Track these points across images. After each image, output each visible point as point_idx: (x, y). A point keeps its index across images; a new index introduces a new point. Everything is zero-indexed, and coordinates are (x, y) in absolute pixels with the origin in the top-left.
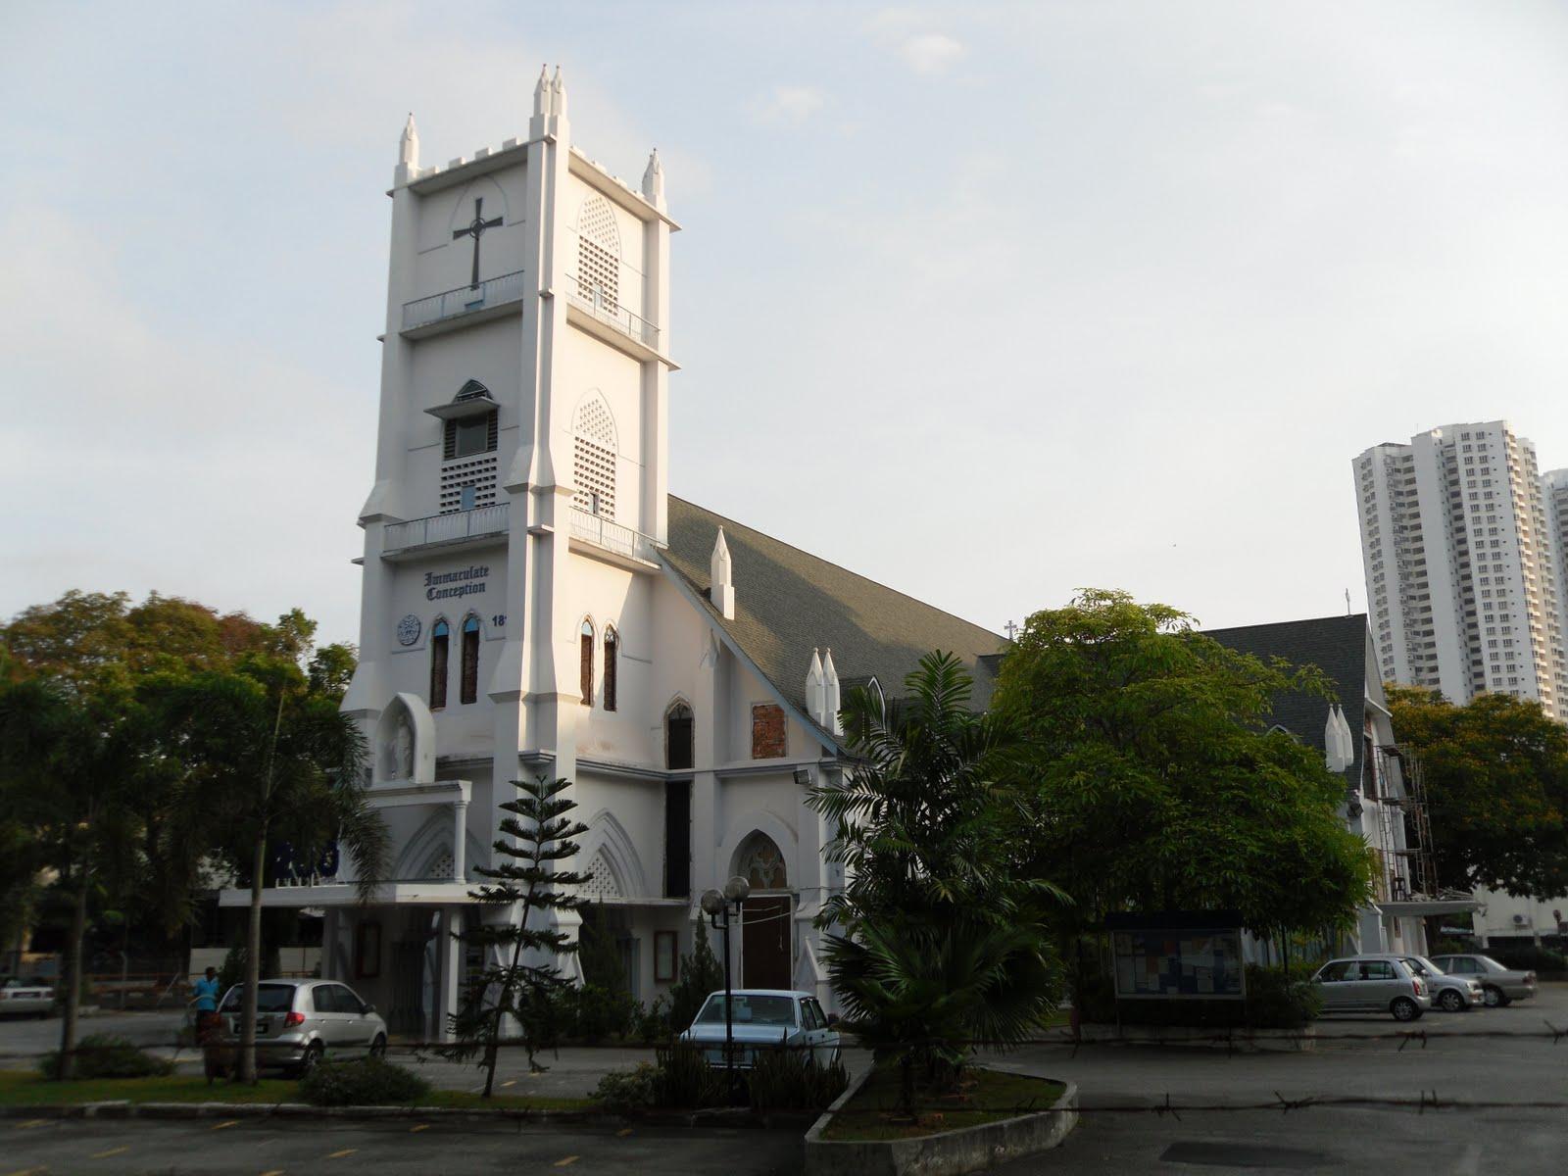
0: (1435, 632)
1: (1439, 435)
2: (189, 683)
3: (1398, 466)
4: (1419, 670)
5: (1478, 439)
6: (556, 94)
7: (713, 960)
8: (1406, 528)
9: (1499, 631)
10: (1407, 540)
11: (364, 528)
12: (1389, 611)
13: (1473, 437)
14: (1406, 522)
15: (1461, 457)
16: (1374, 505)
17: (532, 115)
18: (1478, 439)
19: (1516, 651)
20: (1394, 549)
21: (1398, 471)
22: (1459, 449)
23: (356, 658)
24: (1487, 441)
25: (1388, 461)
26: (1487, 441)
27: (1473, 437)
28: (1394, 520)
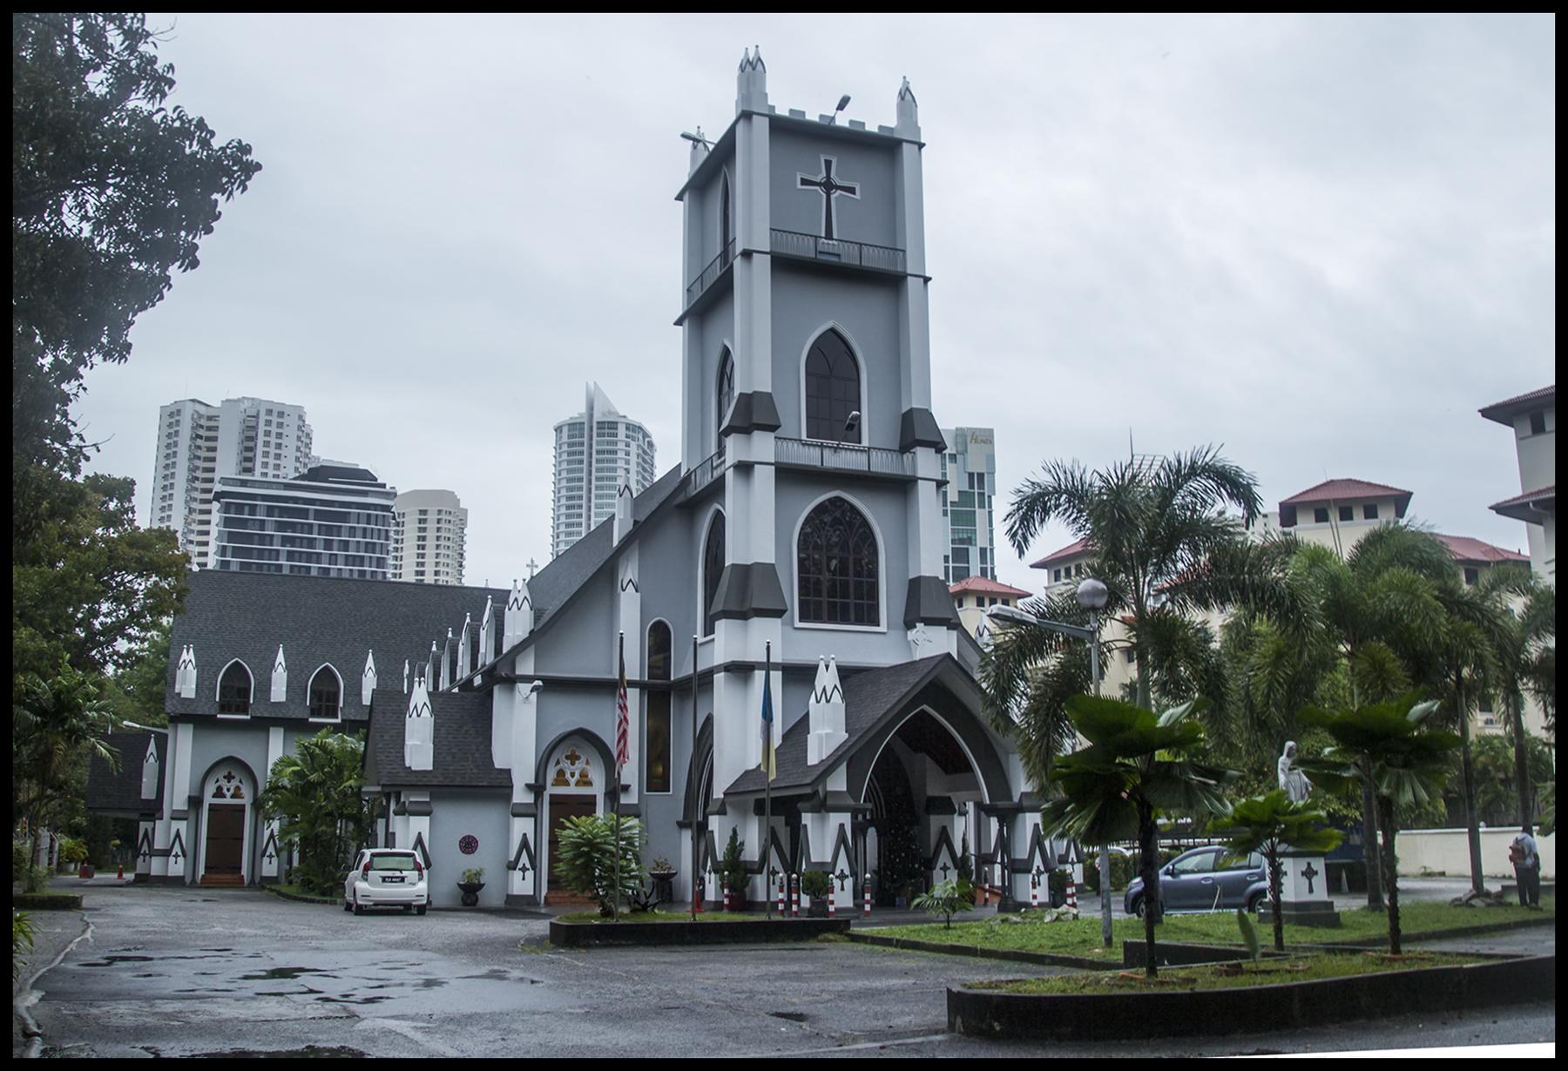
0: (217, 459)
1: (247, 404)
2: (1072, 596)
3: (203, 422)
4: (191, 511)
5: (278, 417)
6: (624, 722)
7: (658, 891)
8: (197, 479)
9: (274, 424)
10: (196, 489)
11: (1541, 524)
12: (172, 519)
13: (275, 414)
14: (199, 474)
15: (262, 428)
16: (172, 484)
17: (1494, 512)
18: (278, 417)
19: (285, 434)
20: (188, 464)
21: (202, 427)
22: (263, 418)
23: (1528, 554)
24: (285, 420)
25: (195, 416)
26: (285, 420)
27: (275, 414)
28: (189, 469)
